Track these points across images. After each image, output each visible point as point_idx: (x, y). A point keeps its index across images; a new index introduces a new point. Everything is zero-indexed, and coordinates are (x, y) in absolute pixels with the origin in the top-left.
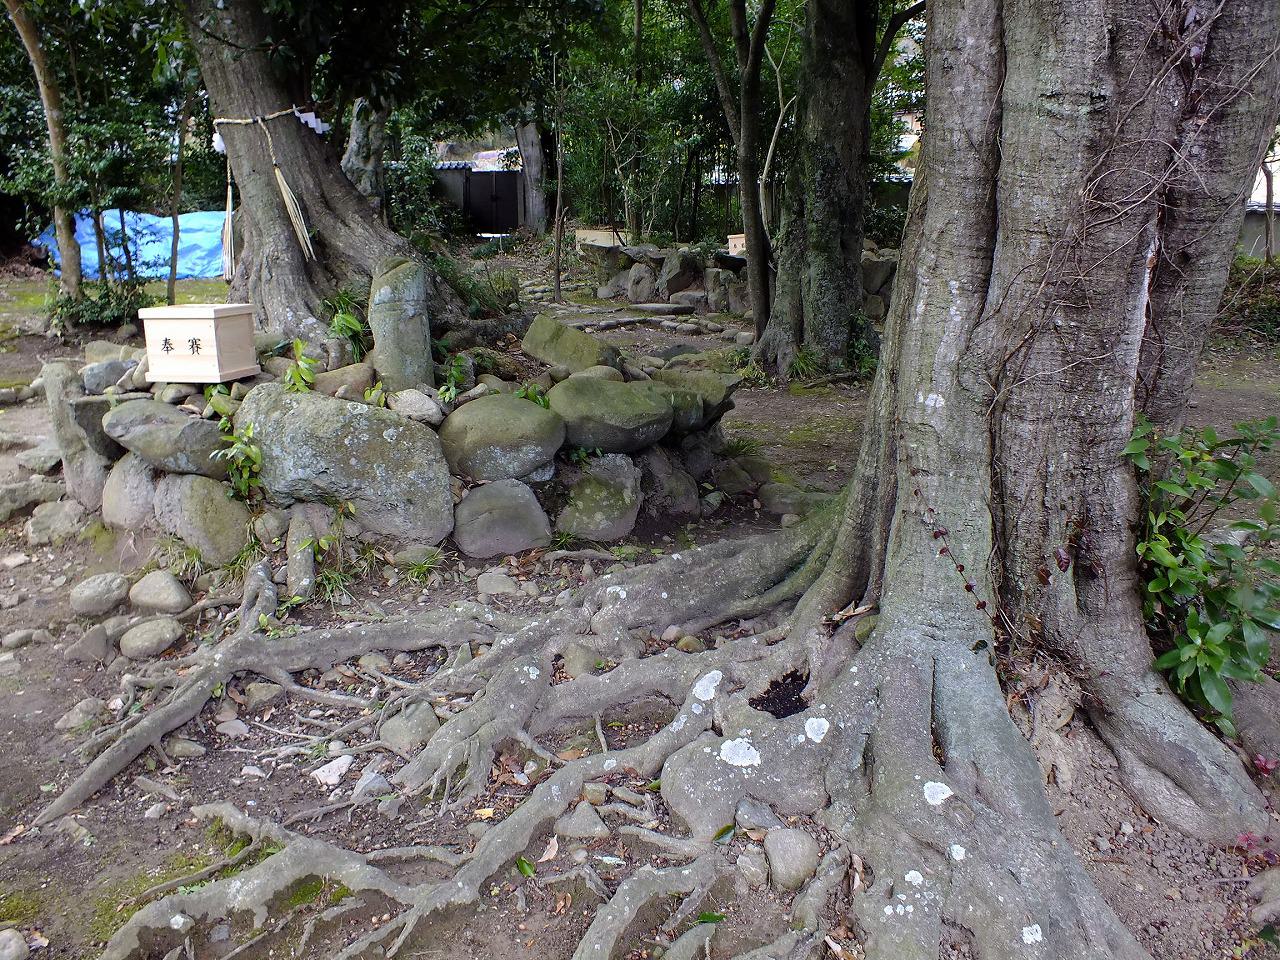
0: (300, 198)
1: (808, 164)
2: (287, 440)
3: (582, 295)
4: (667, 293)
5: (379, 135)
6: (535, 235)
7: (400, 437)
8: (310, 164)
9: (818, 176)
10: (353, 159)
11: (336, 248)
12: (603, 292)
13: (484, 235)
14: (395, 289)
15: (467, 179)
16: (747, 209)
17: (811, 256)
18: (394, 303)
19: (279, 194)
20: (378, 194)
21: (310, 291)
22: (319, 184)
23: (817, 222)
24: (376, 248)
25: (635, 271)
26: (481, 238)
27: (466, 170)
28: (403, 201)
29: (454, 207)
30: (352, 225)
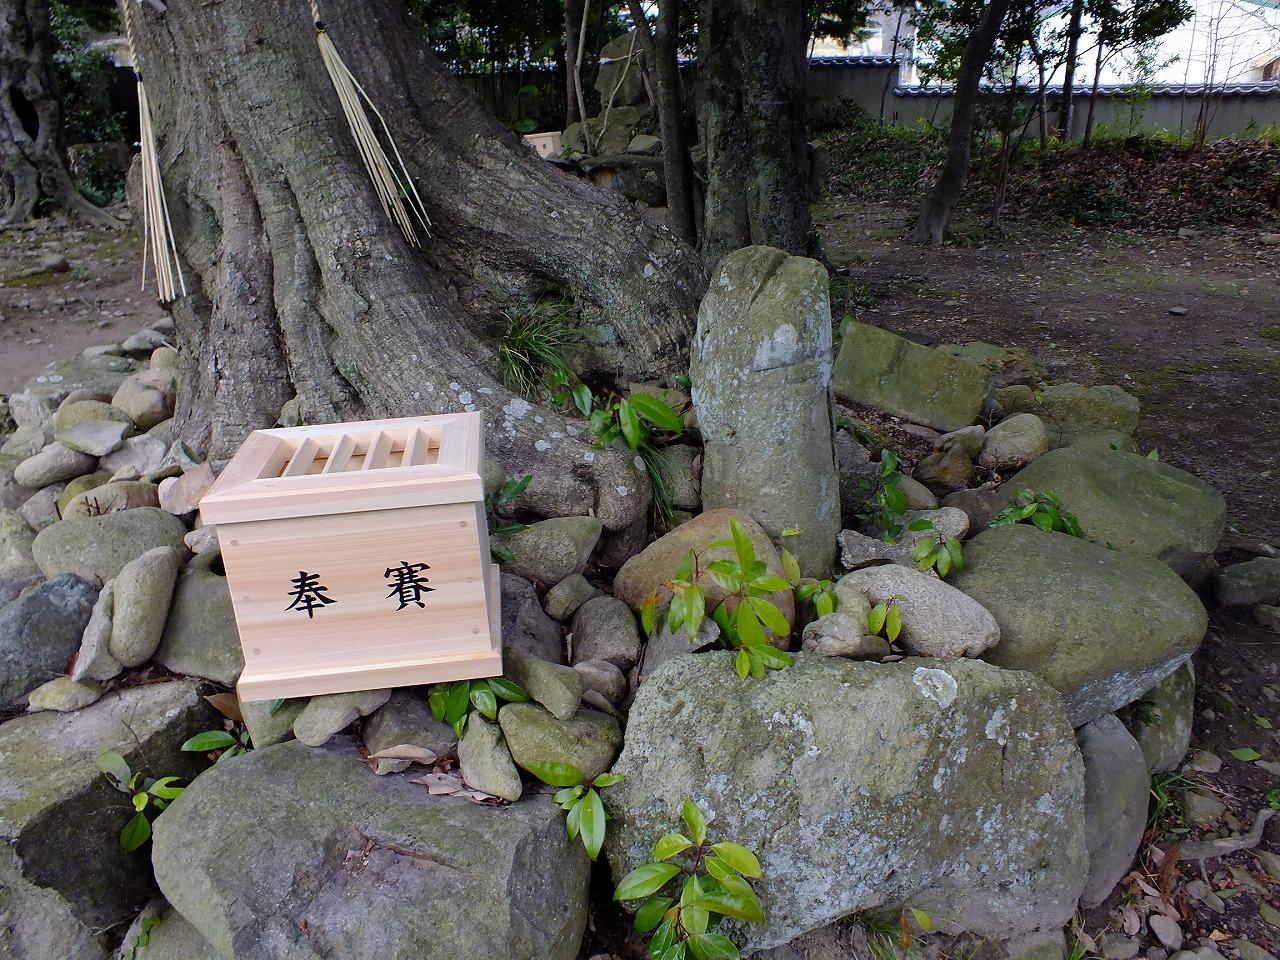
1: (745, 46)
2: (810, 834)
7: (1017, 721)
9: (761, 60)
16: (668, 105)
17: (759, 162)
23: (765, 119)
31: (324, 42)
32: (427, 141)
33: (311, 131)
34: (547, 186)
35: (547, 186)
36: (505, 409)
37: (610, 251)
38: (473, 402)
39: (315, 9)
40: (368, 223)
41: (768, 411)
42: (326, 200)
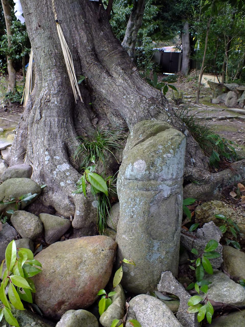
0: (74, 52)
3: (206, 101)
4: (243, 105)
5: (136, 35)
6: (184, 75)
8: (86, 22)
10: (125, 44)
11: (100, 94)
12: (214, 101)
13: (166, 74)
14: (151, 165)
15: (162, 54)
18: (148, 181)
19: (57, 46)
20: (133, 57)
21: (72, 133)
22: (91, 40)
24: (133, 98)
25: (229, 94)
26: (165, 74)
27: (162, 51)
28: (141, 61)
29: (157, 63)
30: (115, 75)
31: (58, 27)
32: (94, 64)
33: (48, 56)
34: (130, 86)
35: (130, 86)
36: (58, 166)
37: (135, 115)
38: (49, 160)
39: (56, 15)
40: (55, 90)
41: (128, 200)
42: (45, 80)
